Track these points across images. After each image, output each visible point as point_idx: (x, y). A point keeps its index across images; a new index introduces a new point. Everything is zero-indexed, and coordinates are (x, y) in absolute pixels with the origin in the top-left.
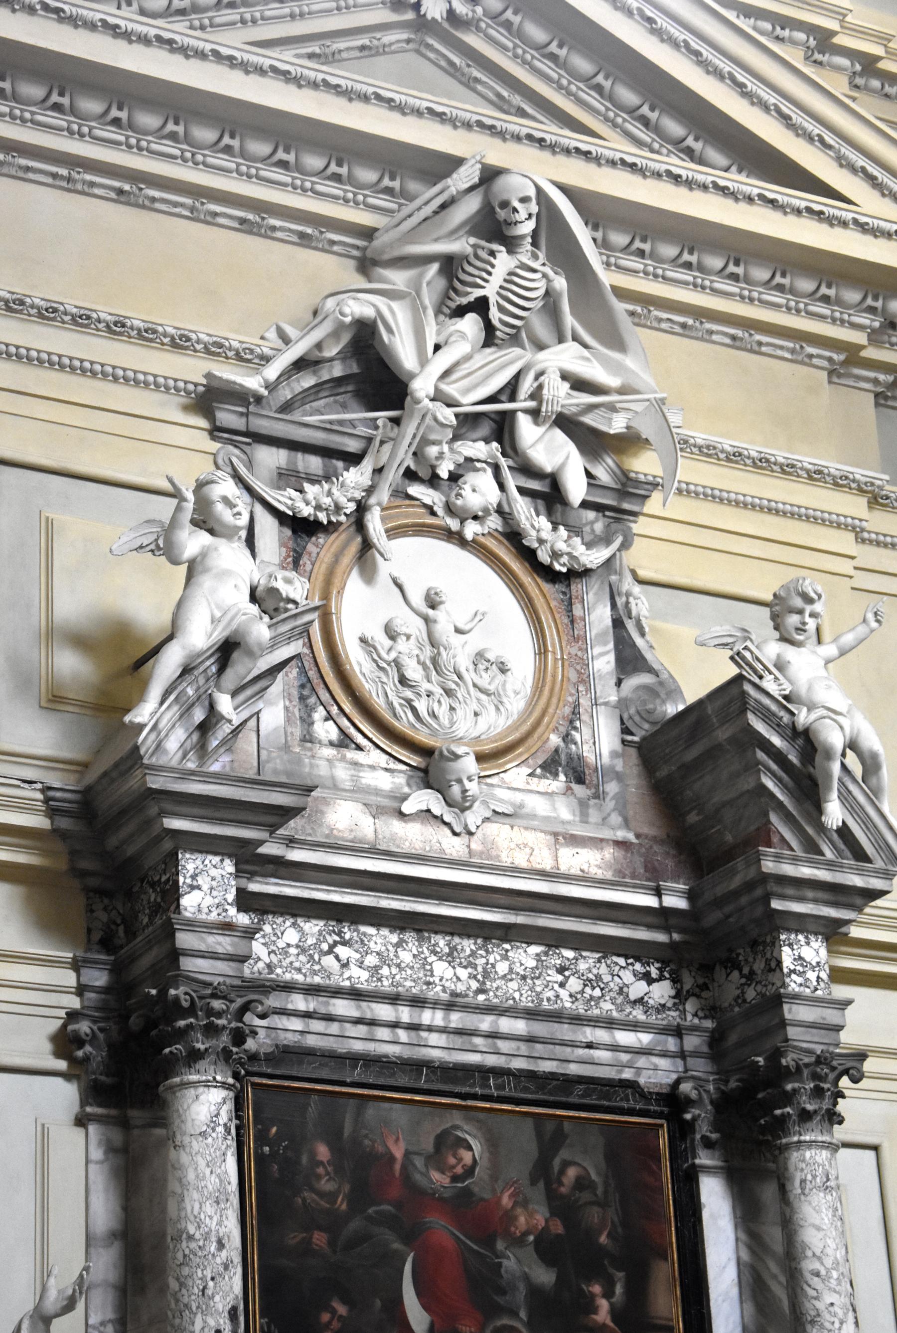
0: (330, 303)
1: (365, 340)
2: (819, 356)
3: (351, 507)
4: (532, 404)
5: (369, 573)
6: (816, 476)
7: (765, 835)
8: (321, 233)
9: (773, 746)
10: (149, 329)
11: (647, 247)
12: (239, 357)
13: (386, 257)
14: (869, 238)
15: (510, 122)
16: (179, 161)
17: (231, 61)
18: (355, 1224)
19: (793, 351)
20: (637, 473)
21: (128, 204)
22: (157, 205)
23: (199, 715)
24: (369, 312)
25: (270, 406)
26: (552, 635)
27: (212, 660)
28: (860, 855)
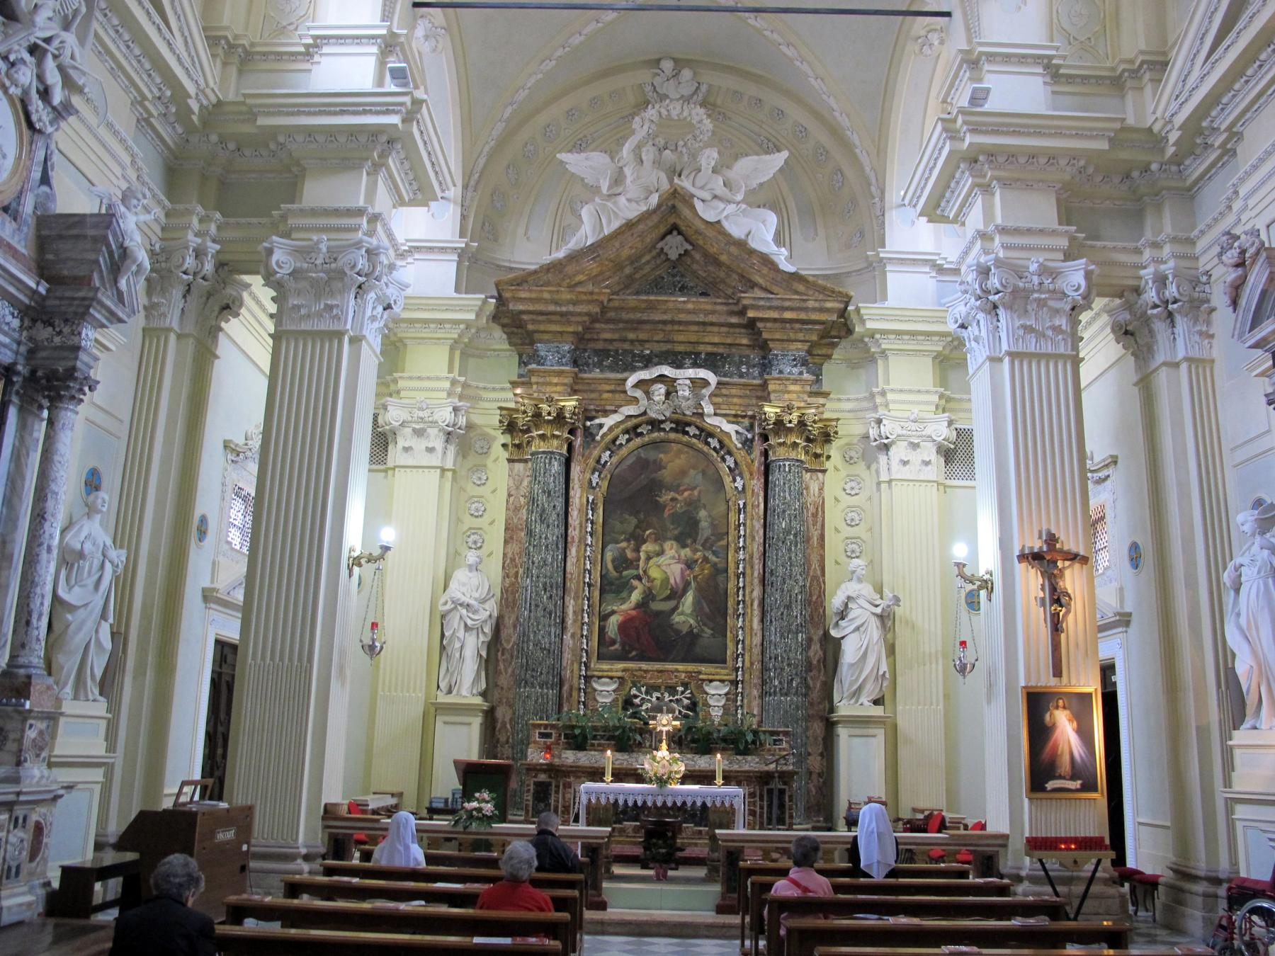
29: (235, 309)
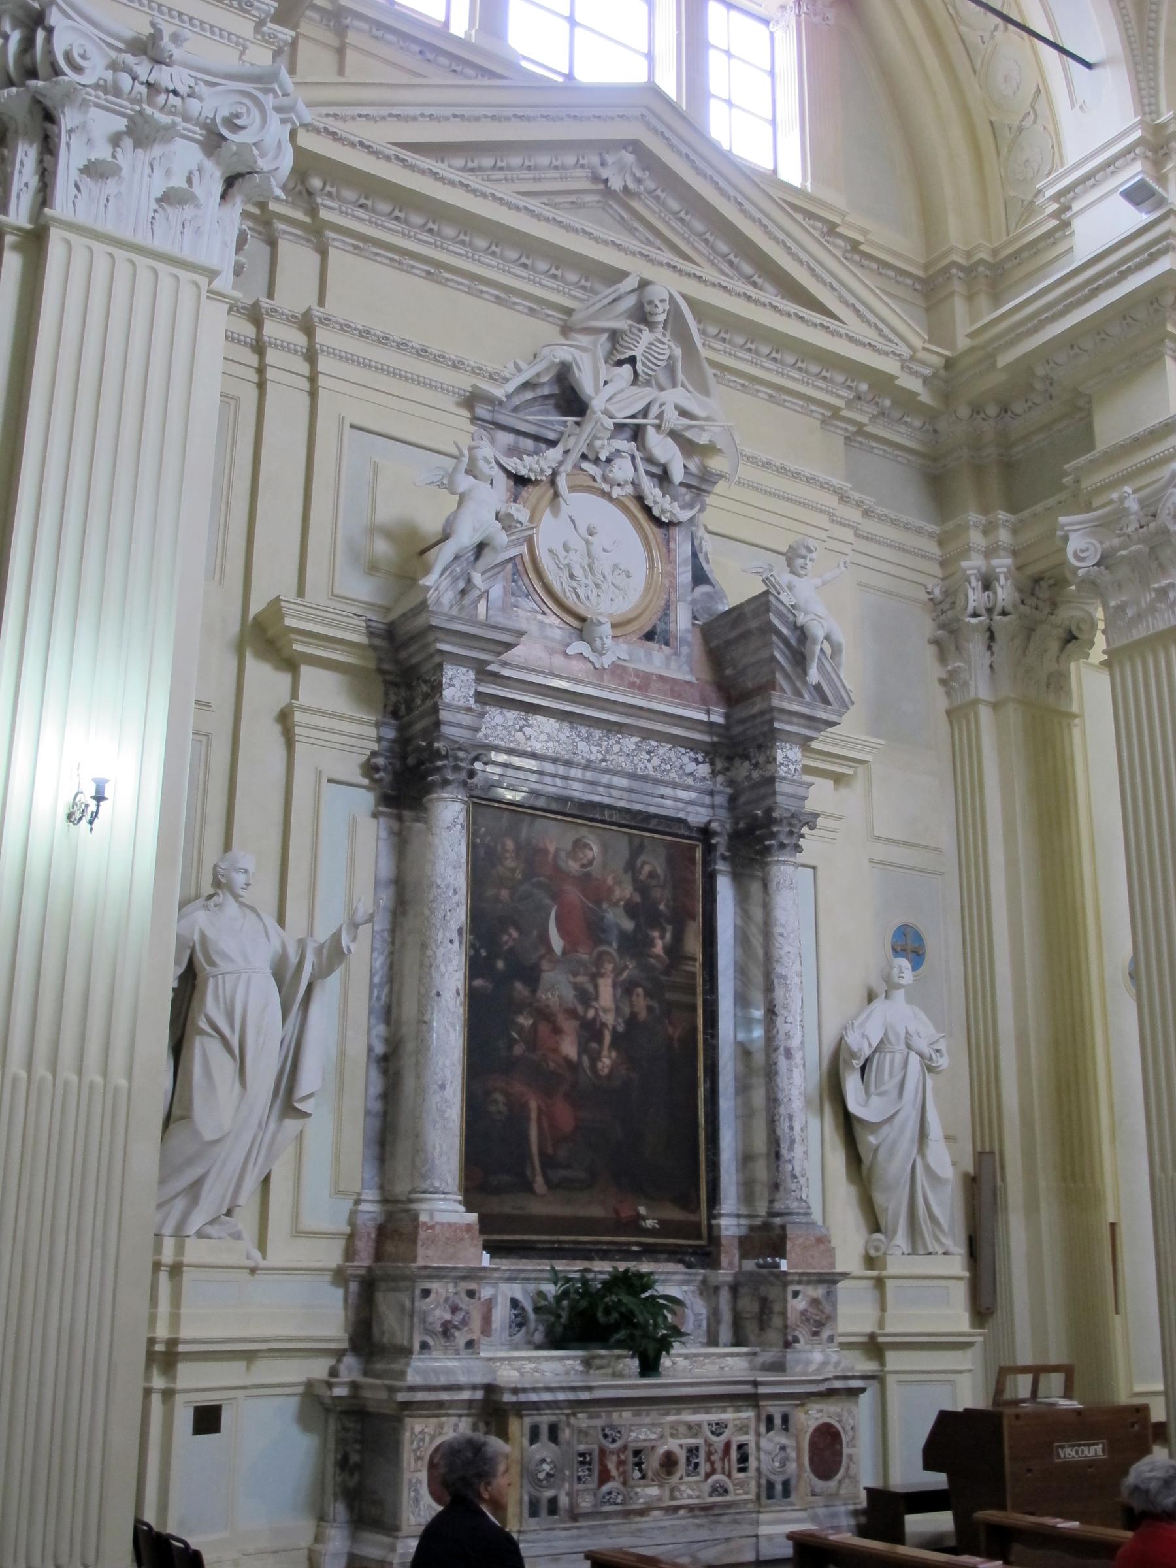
0: (546, 350)
3: (549, 472)
4: (657, 422)
5: (556, 510)
6: (811, 480)
7: (771, 685)
12: (491, 377)
14: (853, 345)
17: (501, 200)
18: (526, 887)
19: (802, 407)
21: (432, 281)
23: (461, 585)
28: (825, 701)
29: (1083, 636)
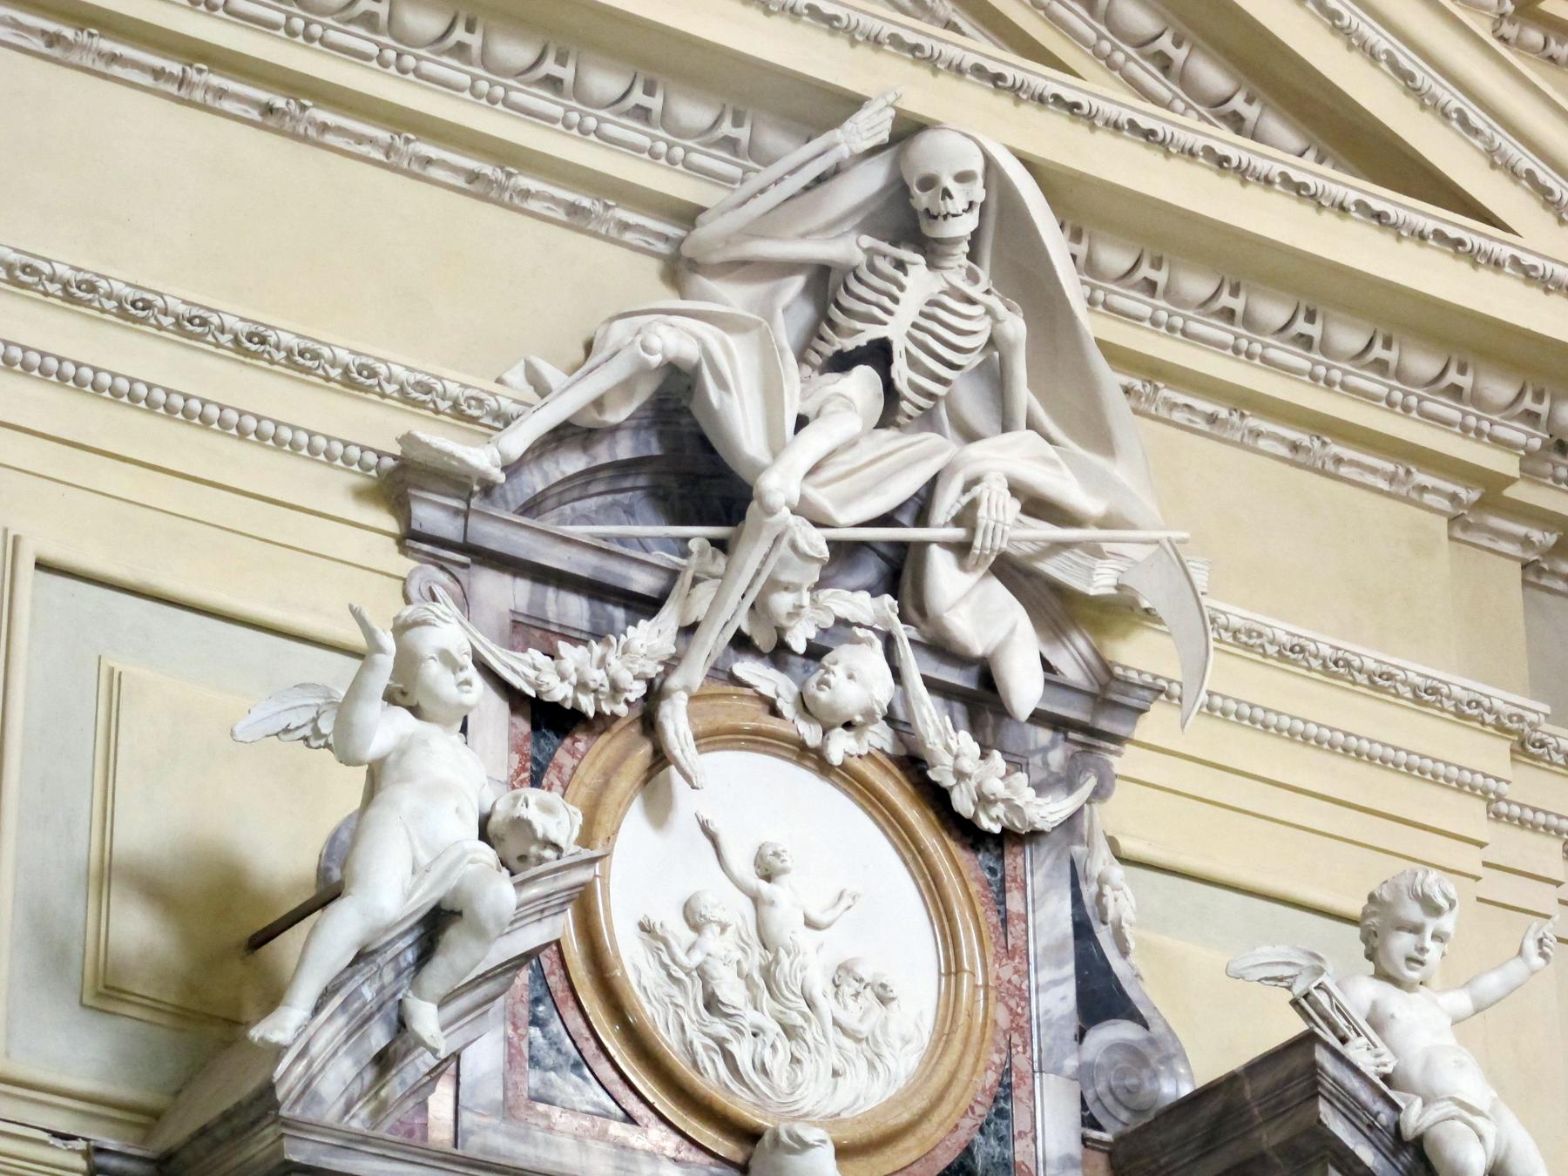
0: (620, 329)
1: (676, 400)
2: (1436, 491)
3: (639, 689)
4: (958, 533)
5: (659, 810)
6: (1426, 697)
8: (607, 207)
9: (1359, 1162)
10: (307, 350)
11: (1160, 277)
12: (458, 412)
13: (716, 258)
14: (1535, 293)
15: (947, 42)
16: (374, 64)
20: (1125, 668)
21: (279, 131)
22: (330, 139)
23: (378, 1037)
24: (689, 351)
25: (506, 502)
26: (969, 943)
27: (409, 940)
